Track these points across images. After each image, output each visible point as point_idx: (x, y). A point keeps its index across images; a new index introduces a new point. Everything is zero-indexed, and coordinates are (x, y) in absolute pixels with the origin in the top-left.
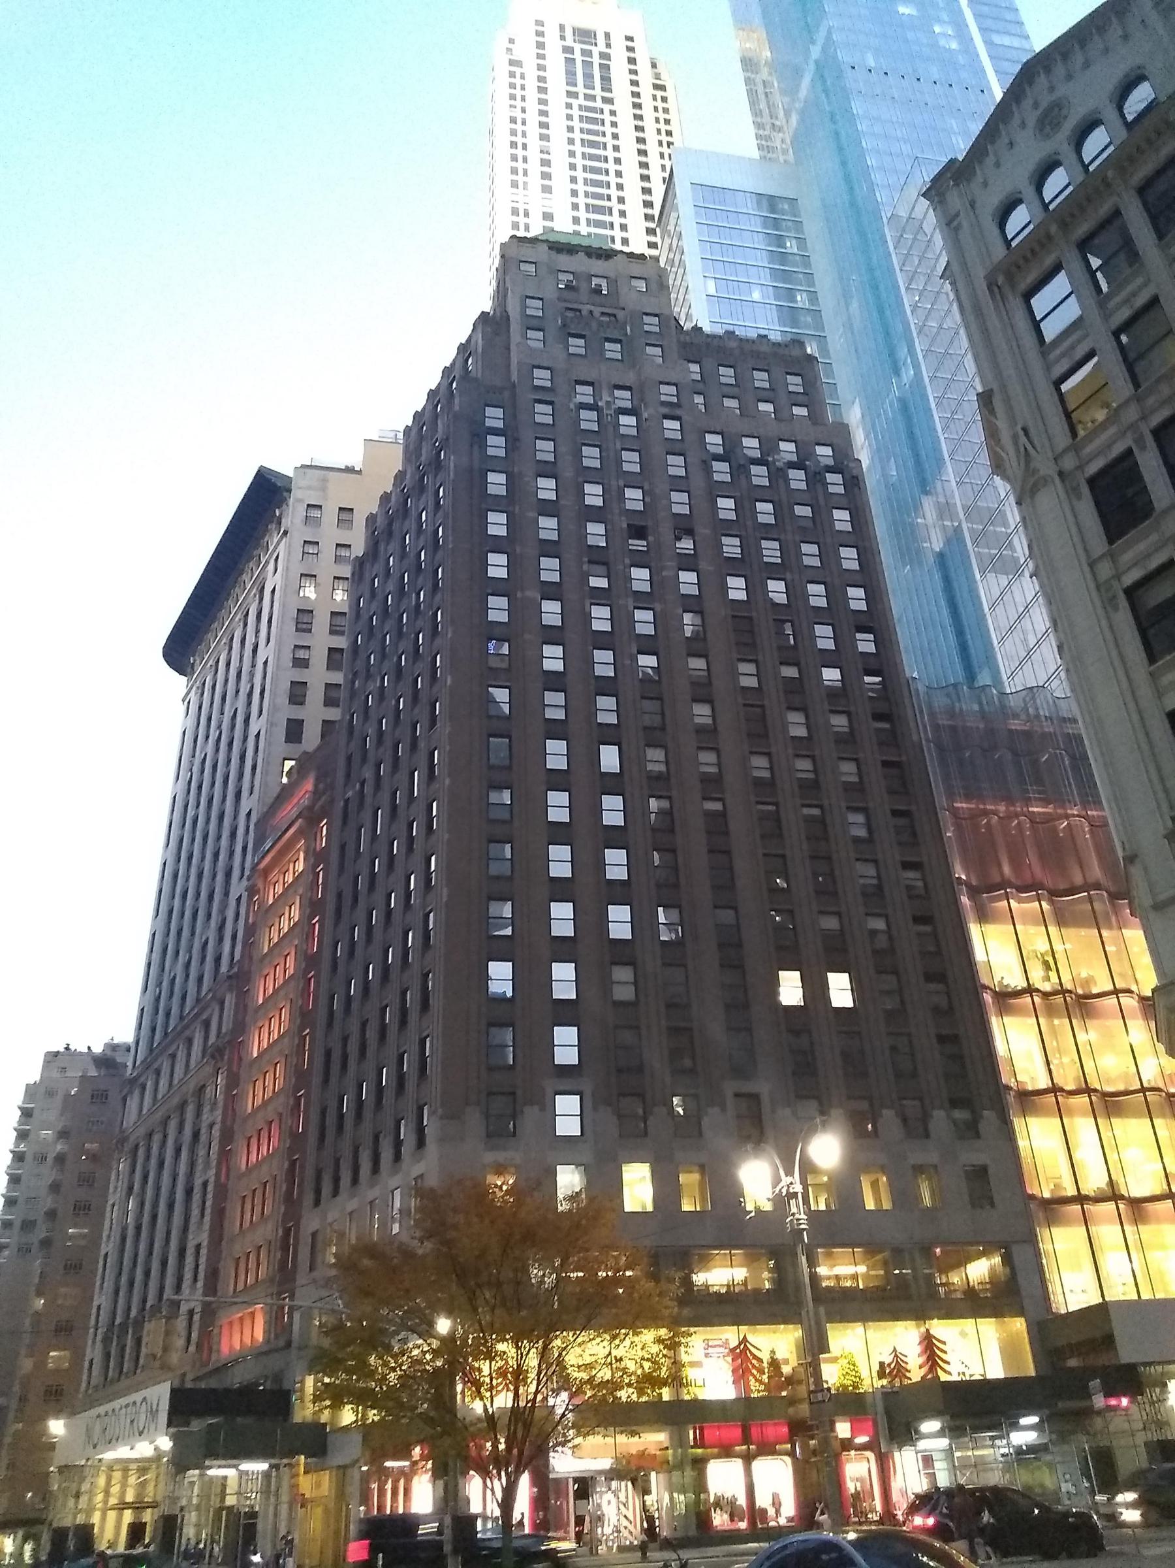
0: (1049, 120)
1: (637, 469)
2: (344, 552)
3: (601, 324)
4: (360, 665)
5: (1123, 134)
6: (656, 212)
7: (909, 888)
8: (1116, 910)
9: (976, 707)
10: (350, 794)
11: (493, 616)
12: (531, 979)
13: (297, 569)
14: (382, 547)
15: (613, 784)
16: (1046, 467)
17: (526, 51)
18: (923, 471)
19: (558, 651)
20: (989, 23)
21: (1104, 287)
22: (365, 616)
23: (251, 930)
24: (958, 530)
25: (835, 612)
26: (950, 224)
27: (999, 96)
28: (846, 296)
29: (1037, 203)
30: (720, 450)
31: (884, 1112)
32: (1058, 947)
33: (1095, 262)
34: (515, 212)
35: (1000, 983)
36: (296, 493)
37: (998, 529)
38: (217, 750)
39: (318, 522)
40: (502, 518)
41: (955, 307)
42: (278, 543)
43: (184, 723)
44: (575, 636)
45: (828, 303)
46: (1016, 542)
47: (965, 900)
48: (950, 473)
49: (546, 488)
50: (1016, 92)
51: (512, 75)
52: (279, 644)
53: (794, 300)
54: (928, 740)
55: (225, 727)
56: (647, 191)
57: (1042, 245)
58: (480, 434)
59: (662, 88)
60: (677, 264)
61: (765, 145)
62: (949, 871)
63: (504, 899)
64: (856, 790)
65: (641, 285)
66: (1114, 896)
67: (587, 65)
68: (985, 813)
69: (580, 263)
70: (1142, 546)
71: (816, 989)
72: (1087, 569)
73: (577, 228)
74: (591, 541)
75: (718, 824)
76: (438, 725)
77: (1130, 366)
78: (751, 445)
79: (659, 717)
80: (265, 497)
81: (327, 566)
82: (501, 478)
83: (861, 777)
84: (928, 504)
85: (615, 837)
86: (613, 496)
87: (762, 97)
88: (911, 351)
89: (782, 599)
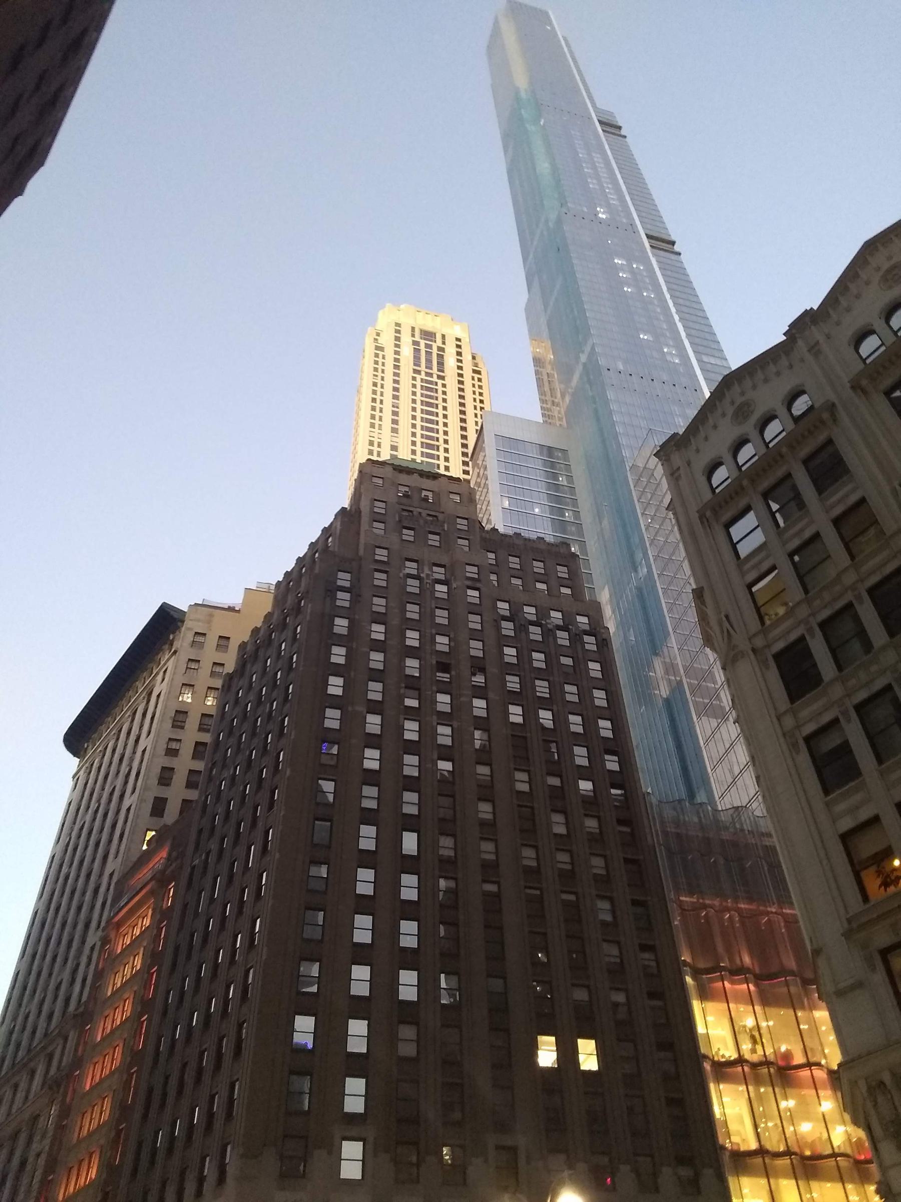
0: (742, 412)
1: (446, 622)
2: (218, 669)
3: (426, 522)
4: (218, 756)
5: (791, 426)
6: (470, 451)
7: (645, 967)
8: (807, 994)
9: (696, 820)
10: (196, 862)
11: (328, 724)
12: (331, 1033)
13: (180, 679)
14: (249, 666)
15: (410, 864)
16: (743, 645)
17: (387, 340)
18: (654, 641)
19: (376, 754)
20: (701, 349)
21: (782, 524)
22: (228, 718)
23: (99, 975)
24: (680, 683)
25: (588, 737)
26: (673, 475)
27: (707, 395)
28: (599, 516)
29: (733, 466)
30: (507, 614)
31: (622, 1167)
32: (763, 1024)
33: (775, 507)
34: (371, 443)
35: (717, 1053)
36: (188, 623)
37: (709, 685)
38: (94, 819)
39: (201, 645)
40: (342, 651)
41: (676, 528)
42: (168, 660)
43: (71, 795)
44: (391, 743)
45: (587, 518)
46: (722, 695)
47: (689, 980)
48: (673, 642)
49: (378, 632)
50: (718, 393)
51: (377, 355)
52: (158, 735)
53: (564, 516)
54: (660, 845)
55: (104, 801)
56: (464, 437)
57: (737, 493)
58: (332, 590)
59: (479, 373)
60: (482, 485)
61: (547, 414)
62: (677, 957)
63: (312, 960)
64: (604, 881)
65: (457, 498)
66: (806, 982)
67: (429, 354)
68: (705, 907)
69: (415, 481)
70: (815, 706)
71: (567, 1053)
72: (775, 720)
73: (413, 457)
74: (408, 671)
75: (493, 903)
76: (275, 808)
77: (801, 578)
78: (530, 611)
79: (452, 812)
80: (164, 624)
81: (203, 678)
82: (345, 622)
83: (608, 871)
84: (658, 664)
85: (409, 910)
86: (427, 640)
87: (546, 384)
88: (645, 554)
89: (549, 724)
